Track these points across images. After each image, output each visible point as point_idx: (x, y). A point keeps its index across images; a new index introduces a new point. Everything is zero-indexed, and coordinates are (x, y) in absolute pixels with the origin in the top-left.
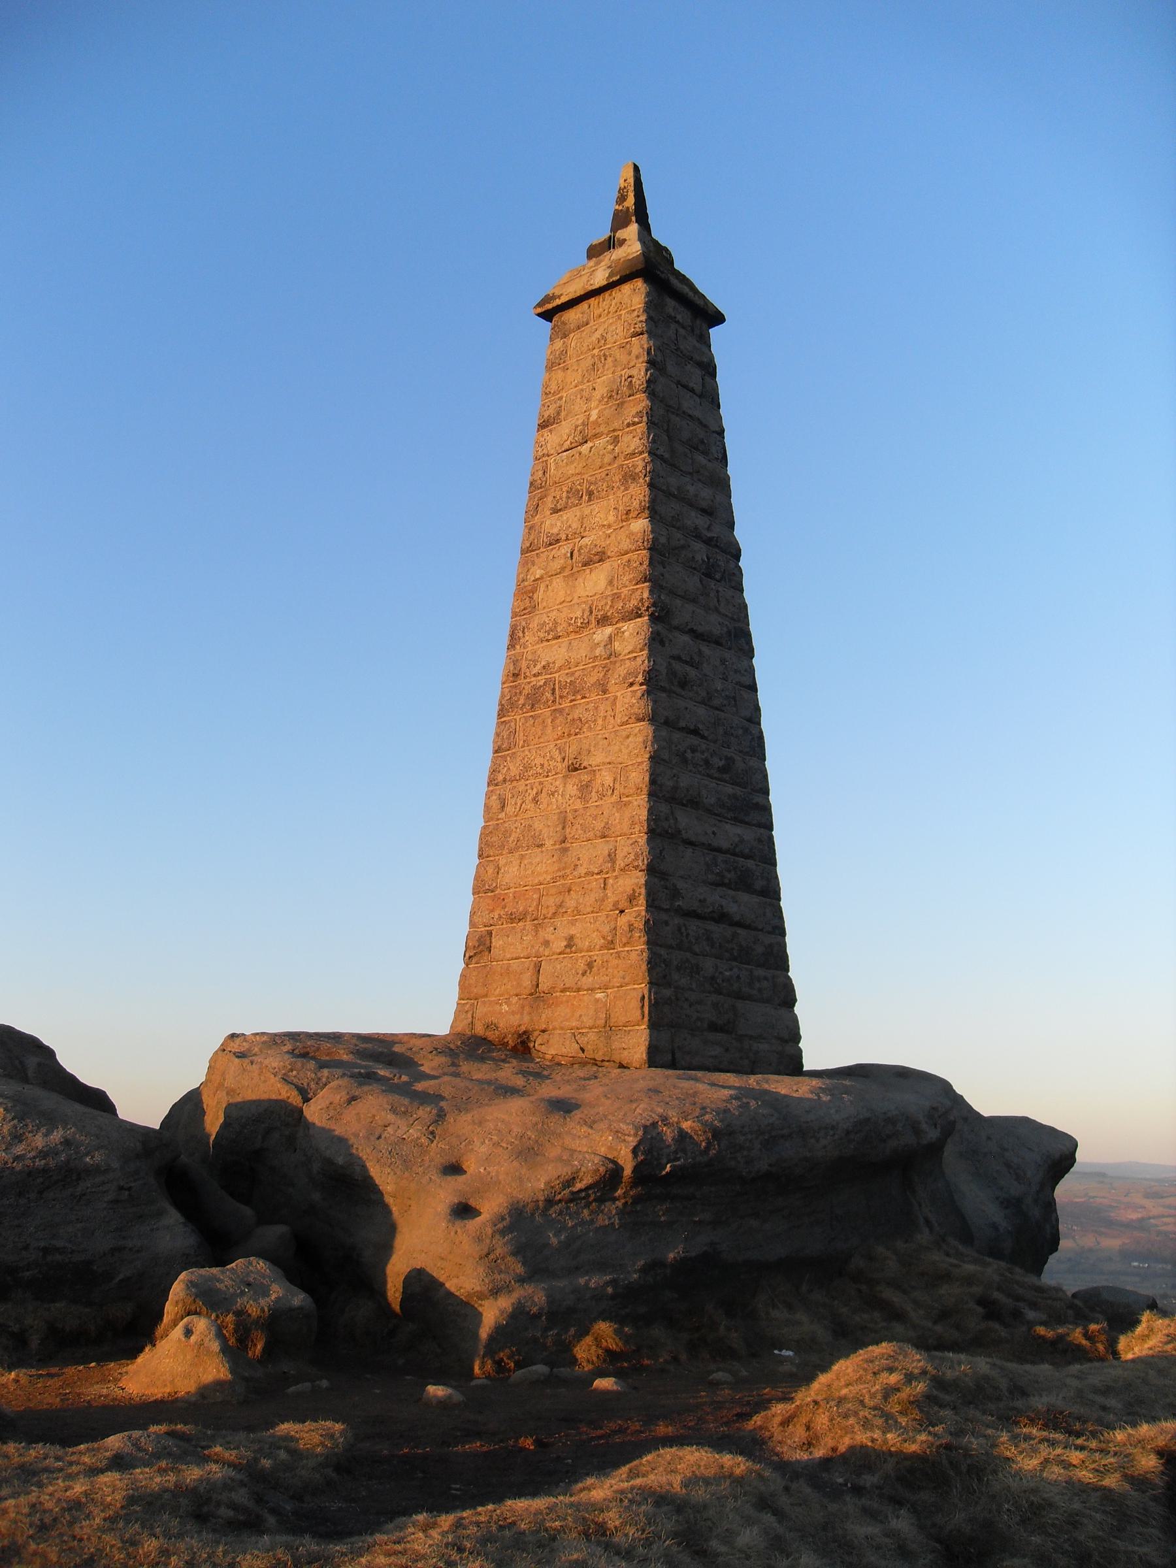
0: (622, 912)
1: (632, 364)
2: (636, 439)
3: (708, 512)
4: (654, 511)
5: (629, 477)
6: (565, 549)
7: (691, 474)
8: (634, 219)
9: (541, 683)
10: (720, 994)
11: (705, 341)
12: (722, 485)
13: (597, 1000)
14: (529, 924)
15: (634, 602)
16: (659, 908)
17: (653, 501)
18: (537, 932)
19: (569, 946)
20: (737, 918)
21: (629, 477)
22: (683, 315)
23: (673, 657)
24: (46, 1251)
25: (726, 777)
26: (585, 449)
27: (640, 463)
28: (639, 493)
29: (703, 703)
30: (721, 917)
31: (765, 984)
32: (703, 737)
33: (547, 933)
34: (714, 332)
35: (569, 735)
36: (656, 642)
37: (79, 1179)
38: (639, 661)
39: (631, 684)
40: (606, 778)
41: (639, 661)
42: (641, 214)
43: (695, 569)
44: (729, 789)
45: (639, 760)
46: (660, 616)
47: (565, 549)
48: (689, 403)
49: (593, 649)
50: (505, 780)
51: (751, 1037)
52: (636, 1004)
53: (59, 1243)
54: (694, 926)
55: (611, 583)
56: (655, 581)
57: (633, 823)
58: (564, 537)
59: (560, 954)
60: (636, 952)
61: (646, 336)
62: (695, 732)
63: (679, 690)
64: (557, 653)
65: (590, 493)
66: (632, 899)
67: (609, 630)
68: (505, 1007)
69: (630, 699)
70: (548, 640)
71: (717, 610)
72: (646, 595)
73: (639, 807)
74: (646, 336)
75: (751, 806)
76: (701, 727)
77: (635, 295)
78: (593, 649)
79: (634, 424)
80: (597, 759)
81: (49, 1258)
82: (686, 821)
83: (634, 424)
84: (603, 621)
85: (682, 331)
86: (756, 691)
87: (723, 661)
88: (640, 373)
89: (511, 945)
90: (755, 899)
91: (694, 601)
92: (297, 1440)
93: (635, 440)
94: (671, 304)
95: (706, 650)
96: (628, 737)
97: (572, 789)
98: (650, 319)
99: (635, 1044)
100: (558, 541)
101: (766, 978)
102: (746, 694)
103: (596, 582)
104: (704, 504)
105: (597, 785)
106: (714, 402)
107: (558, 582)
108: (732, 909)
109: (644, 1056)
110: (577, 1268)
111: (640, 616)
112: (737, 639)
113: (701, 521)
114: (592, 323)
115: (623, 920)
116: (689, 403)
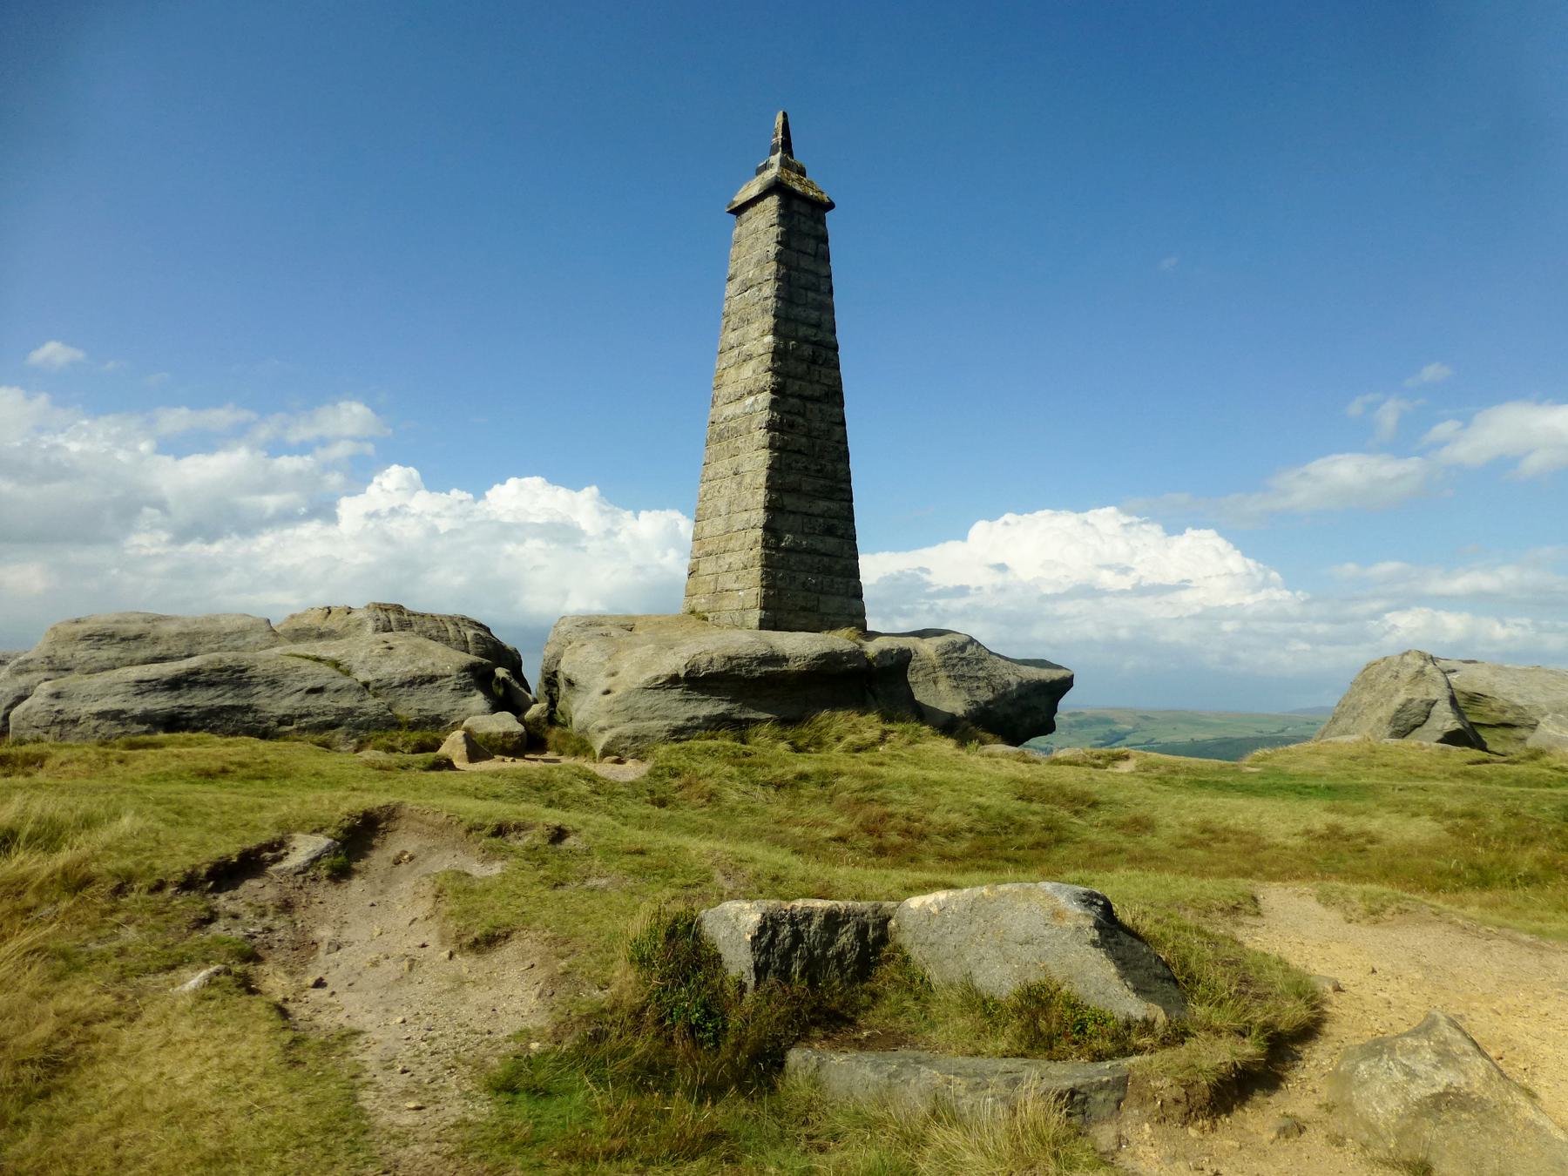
3: (818, 326)
4: (776, 331)
5: (765, 311)
21: (765, 311)
22: (804, 209)
27: (771, 303)
28: (769, 321)
30: (815, 552)
33: (721, 562)
36: (774, 405)
40: (748, 480)
42: (787, 145)
54: (793, 559)
56: (775, 372)
62: (799, 452)
64: (730, 410)
67: (752, 398)
69: (761, 437)
73: (761, 496)
75: (840, 490)
77: (772, 202)
80: (747, 467)
82: (789, 501)
84: (750, 393)
88: (773, 249)
89: (707, 567)
90: (837, 540)
91: (801, 379)
92: (1159, 943)
93: (769, 290)
94: (796, 205)
95: (809, 405)
98: (780, 216)
99: (755, 616)
102: (838, 429)
103: (748, 371)
106: (826, 258)
107: (732, 370)
112: (834, 395)
116: (806, 263)
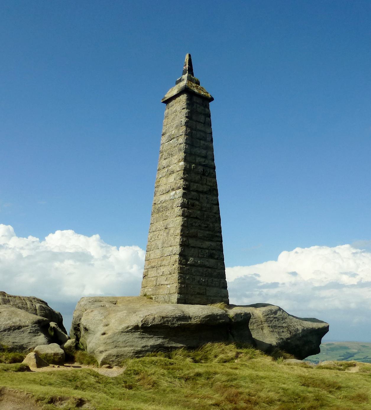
0: (173, 265)
1: (182, 117)
2: (182, 139)
3: (205, 157)
4: (185, 160)
5: (180, 150)
6: (166, 170)
7: (199, 147)
8: (187, 72)
9: (160, 206)
10: (201, 285)
11: (207, 107)
12: (210, 149)
13: (168, 287)
14: (155, 269)
15: (179, 185)
16: (182, 264)
17: (185, 157)
18: (157, 270)
19: (163, 274)
20: (208, 266)
21: (180, 150)
22: (199, 101)
23: (190, 199)
24: (13, 343)
25: (207, 229)
26: (171, 142)
28: (182, 155)
29: (199, 210)
31: (217, 283)
32: (199, 219)
33: (159, 271)
34: (211, 104)
35: (165, 220)
36: (184, 195)
37: (22, 328)
38: (179, 200)
39: (178, 207)
40: (172, 231)
41: (179, 200)
42: (190, 70)
43: (199, 174)
44: (208, 232)
45: (179, 226)
46: (186, 188)
47: (166, 170)
48: (200, 127)
49: (170, 197)
50: (152, 232)
51: (211, 296)
52: (175, 288)
53: (16, 341)
54: (194, 269)
55: (175, 179)
57: (177, 243)
58: (166, 167)
59: (161, 276)
60: (176, 276)
61: (185, 109)
62: (196, 218)
63: (192, 207)
65: (172, 154)
66: (176, 261)
67: (174, 192)
68: (150, 289)
69: (178, 211)
70: (162, 195)
71: (206, 184)
72: (182, 183)
74: (185, 109)
76: (198, 216)
77: (183, 98)
78: (170, 197)
79: (181, 135)
81: (14, 344)
82: (192, 242)
83: (181, 135)
84: (173, 190)
85: (198, 106)
86: (219, 205)
87: (207, 198)
88: (184, 120)
89: (152, 273)
94: (195, 99)
95: (201, 195)
96: (176, 220)
97: (165, 234)
98: (187, 104)
99: (175, 297)
100: (165, 167)
101: (217, 281)
103: (172, 179)
104: (203, 155)
105: (170, 233)
107: (164, 179)
108: (207, 263)
109: (176, 301)
110: (126, 346)
111: (180, 188)
112: (213, 191)
113: (202, 160)
114: (174, 105)
115: (174, 267)
116: (200, 127)
